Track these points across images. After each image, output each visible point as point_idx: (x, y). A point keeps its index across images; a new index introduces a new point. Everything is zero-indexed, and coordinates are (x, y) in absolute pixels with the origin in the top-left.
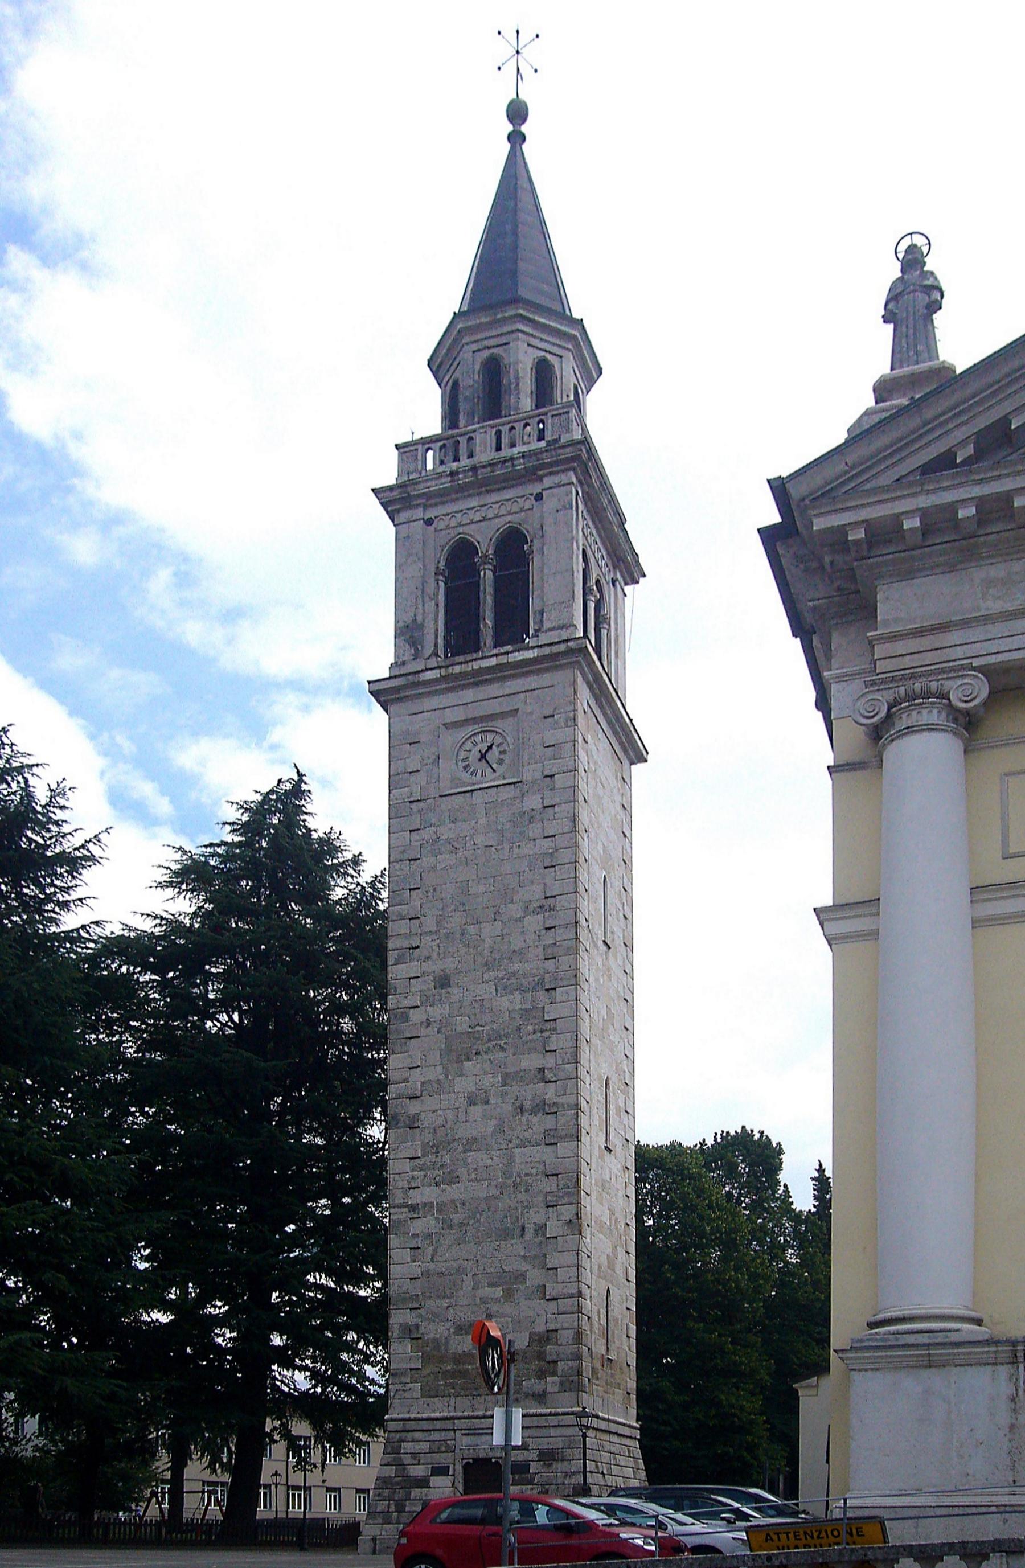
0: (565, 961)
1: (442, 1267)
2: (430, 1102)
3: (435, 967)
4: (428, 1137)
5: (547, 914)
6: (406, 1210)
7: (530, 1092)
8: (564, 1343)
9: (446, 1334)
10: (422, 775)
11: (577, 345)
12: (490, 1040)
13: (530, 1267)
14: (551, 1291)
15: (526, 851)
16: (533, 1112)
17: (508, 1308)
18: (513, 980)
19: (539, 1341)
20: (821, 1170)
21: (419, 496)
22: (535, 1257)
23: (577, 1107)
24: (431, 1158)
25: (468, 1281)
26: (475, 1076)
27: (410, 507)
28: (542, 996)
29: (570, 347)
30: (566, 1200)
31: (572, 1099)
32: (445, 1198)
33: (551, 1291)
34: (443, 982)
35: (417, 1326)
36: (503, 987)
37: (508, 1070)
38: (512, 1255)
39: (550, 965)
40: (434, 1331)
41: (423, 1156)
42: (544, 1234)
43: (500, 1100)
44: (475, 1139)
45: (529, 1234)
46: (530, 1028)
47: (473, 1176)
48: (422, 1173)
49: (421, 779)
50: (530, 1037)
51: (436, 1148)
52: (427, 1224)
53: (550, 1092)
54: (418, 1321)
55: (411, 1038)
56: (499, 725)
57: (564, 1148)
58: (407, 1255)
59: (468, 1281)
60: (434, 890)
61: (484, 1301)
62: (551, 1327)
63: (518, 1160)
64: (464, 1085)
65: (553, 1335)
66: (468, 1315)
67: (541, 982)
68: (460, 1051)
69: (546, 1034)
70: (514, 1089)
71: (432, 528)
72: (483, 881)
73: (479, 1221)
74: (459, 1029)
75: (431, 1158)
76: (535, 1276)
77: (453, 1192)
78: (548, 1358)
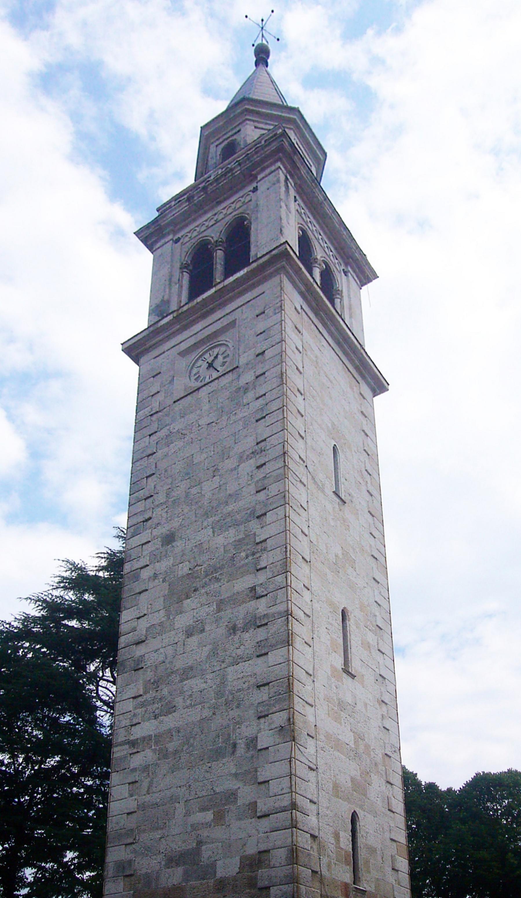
0: (274, 489)
1: (155, 798)
2: (153, 644)
3: (163, 530)
4: (149, 675)
5: (257, 457)
6: (127, 746)
7: (240, 613)
8: (278, 865)
9: (157, 868)
10: (162, 394)
11: (298, 127)
12: (207, 575)
13: (240, 784)
14: (262, 807)
15: (241, 415)
16: (245, 629)
17: (219, 833)
18: (229, 520)
19: (251, 865)
20: (282, 235)
21: (168, 225)
22: (247, 772)
23: (288, 614)
24: (152, 694)
25: (180, 809)
26: (195, 608)
27: (163, 236)
28: (254, 525)
29: (292, 127)
30: (277, 707)
31: (281, 608)
32: (163, 728)
33: (262, 807)
34: (169, 539)
35: (130, 862)
36: (219, 527)
37: (222, 598)
38: (223, 775)
39: (262, 496)
40: (146, 865)
41: (145, 693)
42: (255, 746)
43: (215, 625)
44: (191, 668)
45: (241, 750)
46: (243, 554)
47: (189, 702)
48: (143, 709)
49: (160, 397)
50: (243, 562)
51: (156, 684)
52: (147, 756)
53: (261, 607)
54: (131, 856)
55: (140, 593)
56: (222, 339)
57: (275, 656)
58: (125, 790)
59: (180, 809)
60: (166, 471)
61: (195, 827)
62: (263, 847)
63: (230, 678)
64: (183, 621)
65: (264, 857)
66: (178, 844)
67: (253, 512)
68: (179, 593)
69: (258, 555)
70: (227, 614)
71: (179, 243)
72: (205, 450)
73: (192, 745)
74: (180, 573)
75: (152, 694)
76: (246, 793)
77: (170, 722)
78: (260, 884)
